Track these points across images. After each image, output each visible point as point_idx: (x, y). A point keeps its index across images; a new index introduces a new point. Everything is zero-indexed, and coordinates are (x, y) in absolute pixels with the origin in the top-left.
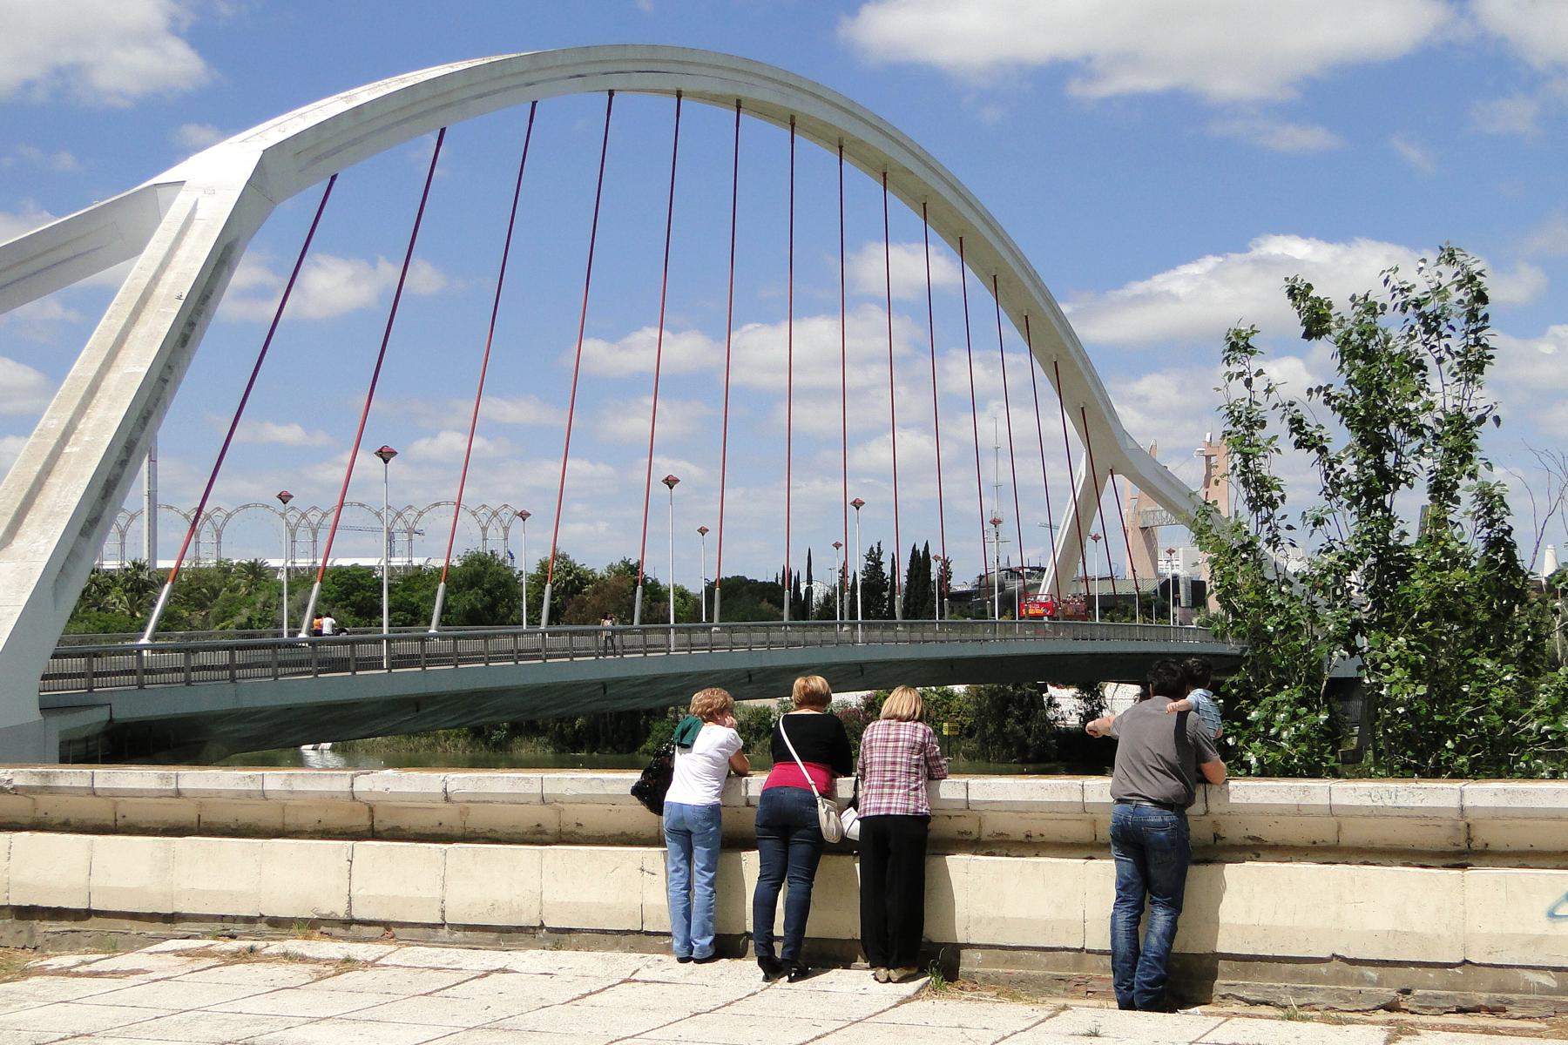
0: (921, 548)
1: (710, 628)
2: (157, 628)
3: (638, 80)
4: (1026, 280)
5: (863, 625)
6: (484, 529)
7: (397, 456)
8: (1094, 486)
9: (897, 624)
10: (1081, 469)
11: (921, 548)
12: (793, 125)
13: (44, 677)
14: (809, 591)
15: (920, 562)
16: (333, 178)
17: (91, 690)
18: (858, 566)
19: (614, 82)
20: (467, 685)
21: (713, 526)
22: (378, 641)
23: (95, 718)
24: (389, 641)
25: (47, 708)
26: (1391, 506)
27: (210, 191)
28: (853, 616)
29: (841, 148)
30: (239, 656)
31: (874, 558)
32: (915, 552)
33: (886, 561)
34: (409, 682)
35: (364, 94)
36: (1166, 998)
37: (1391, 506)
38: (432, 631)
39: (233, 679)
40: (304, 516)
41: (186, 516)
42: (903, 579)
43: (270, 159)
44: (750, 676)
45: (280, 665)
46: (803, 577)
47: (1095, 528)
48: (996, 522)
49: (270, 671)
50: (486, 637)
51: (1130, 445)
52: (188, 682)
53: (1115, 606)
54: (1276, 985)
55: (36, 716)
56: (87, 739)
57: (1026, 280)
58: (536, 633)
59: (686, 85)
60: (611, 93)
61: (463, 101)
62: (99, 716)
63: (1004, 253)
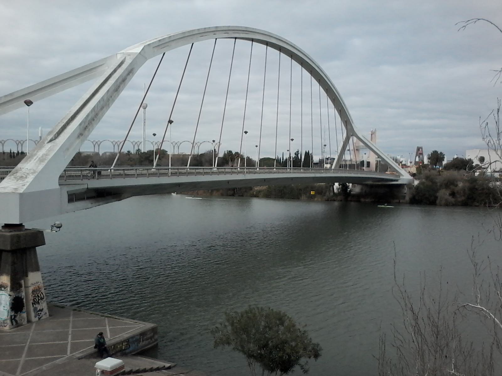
0: (307, 152)
1: (237, 168)
2: (115, 165)
5: (293, 168)
8: (348, 139)
9: (274, 168)
10: (345, 135)
11: (307, 152)
15: (307, 154)
18: (293, 155)
26: (168, 124)
27: (129, 54)
28: (291, 167)
31: (297, 154)
32: (306, 152)
33: (299, 156)
37: (168, 124)
38: (154, 167)
41: (192, 143)
42: (303, 160)
44: (265, 180)
47: (348, 148)
48: (325, 145)
50: (81, 170)
53: (352, 167)
54: (128, 332)
58: (185, 169)
60: (216, 39)
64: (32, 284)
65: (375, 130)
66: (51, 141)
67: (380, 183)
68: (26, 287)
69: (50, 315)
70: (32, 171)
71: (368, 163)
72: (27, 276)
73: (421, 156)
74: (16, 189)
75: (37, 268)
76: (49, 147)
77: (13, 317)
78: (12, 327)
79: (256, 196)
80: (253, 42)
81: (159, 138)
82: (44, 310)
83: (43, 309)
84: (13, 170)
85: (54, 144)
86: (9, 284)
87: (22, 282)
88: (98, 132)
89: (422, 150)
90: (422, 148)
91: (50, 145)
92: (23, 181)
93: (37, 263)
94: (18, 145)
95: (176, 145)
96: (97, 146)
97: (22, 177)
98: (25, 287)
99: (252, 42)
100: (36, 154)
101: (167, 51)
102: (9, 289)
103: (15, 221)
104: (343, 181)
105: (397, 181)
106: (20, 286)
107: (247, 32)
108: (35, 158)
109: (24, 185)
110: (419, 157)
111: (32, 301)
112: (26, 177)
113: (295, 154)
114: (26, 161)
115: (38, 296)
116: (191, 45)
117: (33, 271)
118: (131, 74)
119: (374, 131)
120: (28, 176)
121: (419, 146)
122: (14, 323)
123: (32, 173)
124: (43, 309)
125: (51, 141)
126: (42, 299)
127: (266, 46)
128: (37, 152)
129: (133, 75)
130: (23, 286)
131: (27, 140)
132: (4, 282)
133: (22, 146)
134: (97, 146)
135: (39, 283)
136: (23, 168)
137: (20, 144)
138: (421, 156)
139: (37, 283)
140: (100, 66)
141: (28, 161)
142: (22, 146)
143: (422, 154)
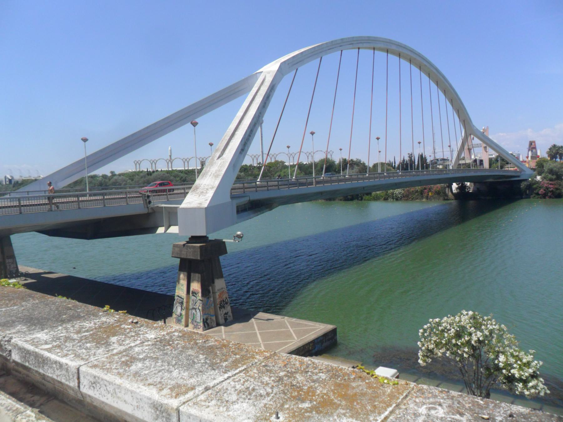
3: (365, 45)
4: (452, 91)
6: (308, 157)
7: (113, 170)
12: (400, 55)
13: (232, 189)
14: (395, 165)
16: (297, 70)
17: (244, 192)
19: (360, 45)
20: (334, 188)
21: (422, 141)
22: (313, 178)
23: (244, 200)
24: (315, 178)
25: (233, 197)
27: (269, 73)
29: (410, 61)
30: (280, 183)
31: (411, 156)
34: (320, 188)
35: (302, 50)
36: (21, 396)
39: (279, 189)
40: (255, 156)
43: (282, 64)
45: (290, 184)
46: (394, 163)
49: (287, 186)
51: (475, 128)
52: (268, 190)
55: (229, 200)
56: (245, 204)
57: (452, 91)
59: (376, 46)
60: (342, 51)
61: (326, 51)
62: (247, 199)
63: (447, 84)
64: (218, 290)
65: (488, 127)
66: (219, 157)
67: (501, 180)
68: (214, 293)
69: (234, 318)
70: (210, 186)
71: (481, 161)
72: (213, 282)
73: (534, 150)
74: (200, 204)
75: (221, 276)
76: (220, 163)
77: (205, 320)
78: (205, 329)
79: (377, 199)
80: (375, 51)
81: (295, 149)
82: (229, 314)
83: (228, 313)
84: (194, 186)
85: (222, 161)
86: (200, 290)
87: (210, 288)
88: (254, 149)
89: (535, 145)
90: (534, 142)
91: (220, 161)
92: (205, 195)
93: (221, 272)
94: (136, 165)
95: (255, 158)
96: (186, 164)
97: (202, 192)
98: (213, 293)
99: (373, 51)
100: (209, 171)
101: (345, 49)
102: (200, 295)
103: (201, 232)
104: (460, 180)
105: (519, 177)
106: (209, 292)
107: (370, 42)
108: (209, 174)
109: (207, 200)
110: (532, 151)
111: (219, 306)
112: (206, 193)
113: (409, 157)
114: (202, 178)
115: (224, 301)
116: (320, 58)
117: (218, 278)
118: (273, 91)
119: (486, 128)
120: (208, 192)
121: (532, 140)
122: (206, 326)
123: (210, 188)
124: (228, 313)
125: (219, 157)
126: (227, 303)
127: (386, 54)
128: (210, 168)
129: (274, 91)
130: (211, 292)
131: (88, 167)
132: (195, 288)
133: (188, 163)
134: (186, 164)
135: (224, 289)
136: (201, 184)
137: (153, 163)
138: (534, 150)
139: (222, 289)
140: (239, 91)
141: (204, 177)
142: (188, 163)
143: (535, 148)
